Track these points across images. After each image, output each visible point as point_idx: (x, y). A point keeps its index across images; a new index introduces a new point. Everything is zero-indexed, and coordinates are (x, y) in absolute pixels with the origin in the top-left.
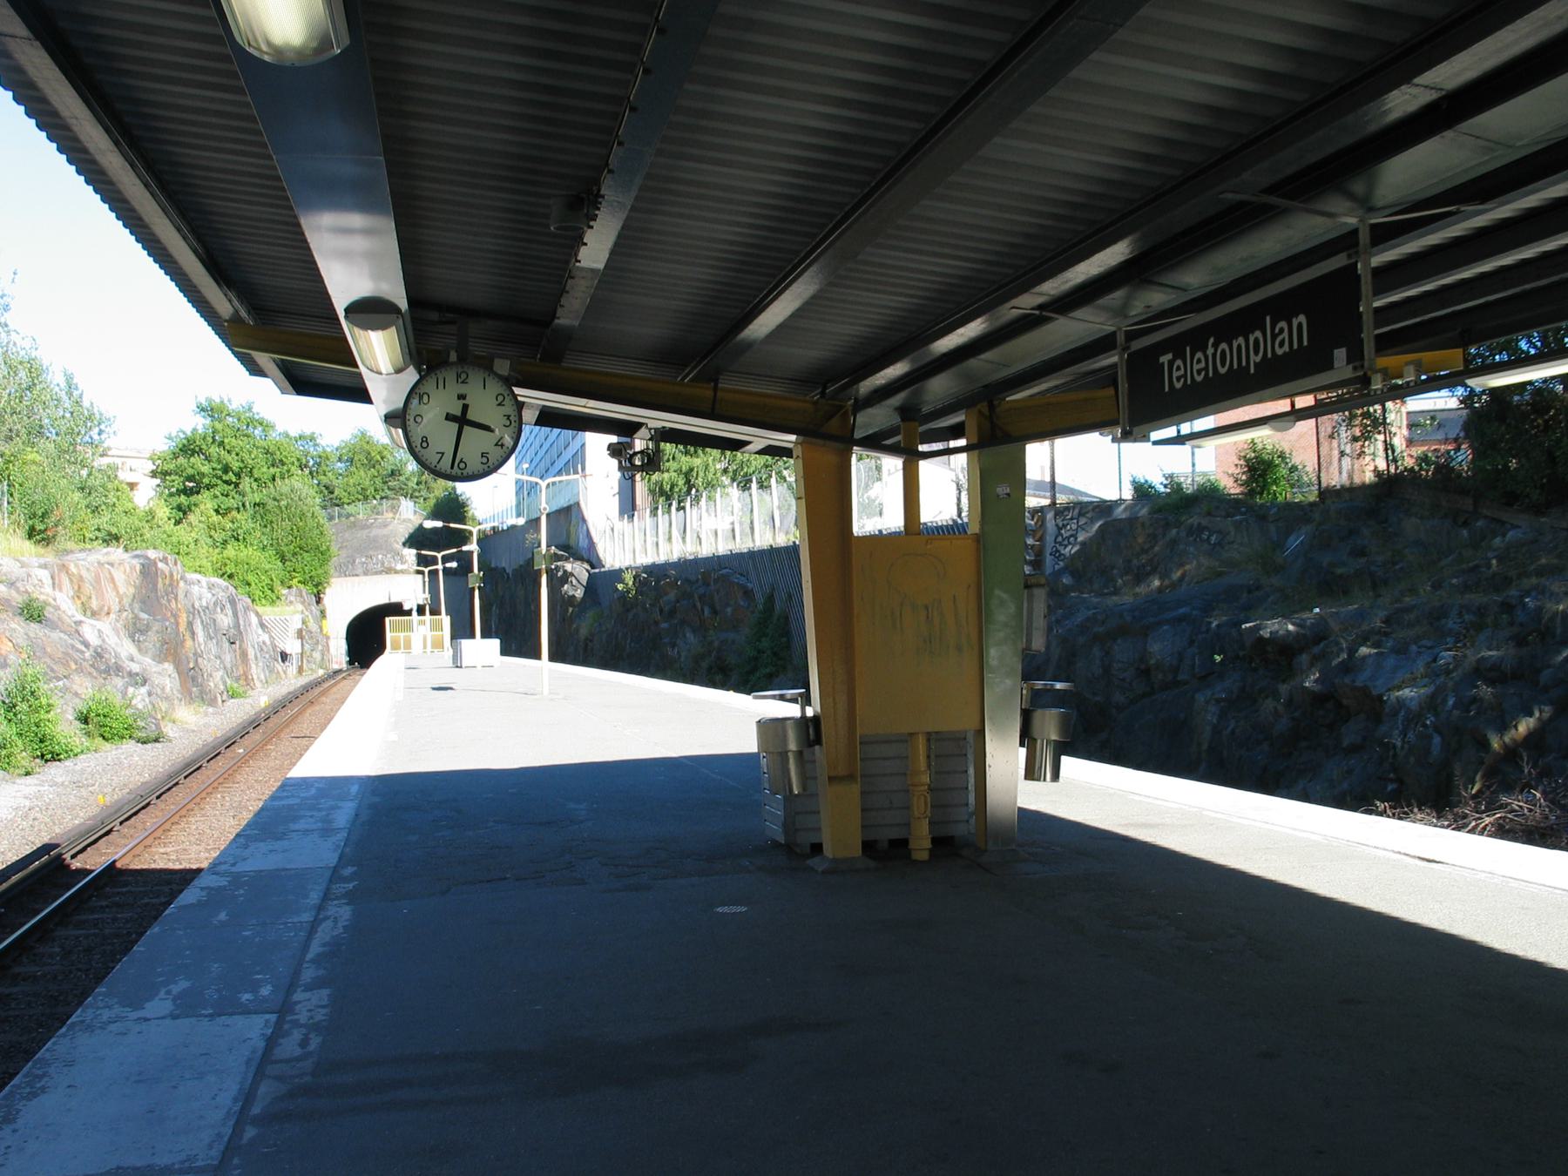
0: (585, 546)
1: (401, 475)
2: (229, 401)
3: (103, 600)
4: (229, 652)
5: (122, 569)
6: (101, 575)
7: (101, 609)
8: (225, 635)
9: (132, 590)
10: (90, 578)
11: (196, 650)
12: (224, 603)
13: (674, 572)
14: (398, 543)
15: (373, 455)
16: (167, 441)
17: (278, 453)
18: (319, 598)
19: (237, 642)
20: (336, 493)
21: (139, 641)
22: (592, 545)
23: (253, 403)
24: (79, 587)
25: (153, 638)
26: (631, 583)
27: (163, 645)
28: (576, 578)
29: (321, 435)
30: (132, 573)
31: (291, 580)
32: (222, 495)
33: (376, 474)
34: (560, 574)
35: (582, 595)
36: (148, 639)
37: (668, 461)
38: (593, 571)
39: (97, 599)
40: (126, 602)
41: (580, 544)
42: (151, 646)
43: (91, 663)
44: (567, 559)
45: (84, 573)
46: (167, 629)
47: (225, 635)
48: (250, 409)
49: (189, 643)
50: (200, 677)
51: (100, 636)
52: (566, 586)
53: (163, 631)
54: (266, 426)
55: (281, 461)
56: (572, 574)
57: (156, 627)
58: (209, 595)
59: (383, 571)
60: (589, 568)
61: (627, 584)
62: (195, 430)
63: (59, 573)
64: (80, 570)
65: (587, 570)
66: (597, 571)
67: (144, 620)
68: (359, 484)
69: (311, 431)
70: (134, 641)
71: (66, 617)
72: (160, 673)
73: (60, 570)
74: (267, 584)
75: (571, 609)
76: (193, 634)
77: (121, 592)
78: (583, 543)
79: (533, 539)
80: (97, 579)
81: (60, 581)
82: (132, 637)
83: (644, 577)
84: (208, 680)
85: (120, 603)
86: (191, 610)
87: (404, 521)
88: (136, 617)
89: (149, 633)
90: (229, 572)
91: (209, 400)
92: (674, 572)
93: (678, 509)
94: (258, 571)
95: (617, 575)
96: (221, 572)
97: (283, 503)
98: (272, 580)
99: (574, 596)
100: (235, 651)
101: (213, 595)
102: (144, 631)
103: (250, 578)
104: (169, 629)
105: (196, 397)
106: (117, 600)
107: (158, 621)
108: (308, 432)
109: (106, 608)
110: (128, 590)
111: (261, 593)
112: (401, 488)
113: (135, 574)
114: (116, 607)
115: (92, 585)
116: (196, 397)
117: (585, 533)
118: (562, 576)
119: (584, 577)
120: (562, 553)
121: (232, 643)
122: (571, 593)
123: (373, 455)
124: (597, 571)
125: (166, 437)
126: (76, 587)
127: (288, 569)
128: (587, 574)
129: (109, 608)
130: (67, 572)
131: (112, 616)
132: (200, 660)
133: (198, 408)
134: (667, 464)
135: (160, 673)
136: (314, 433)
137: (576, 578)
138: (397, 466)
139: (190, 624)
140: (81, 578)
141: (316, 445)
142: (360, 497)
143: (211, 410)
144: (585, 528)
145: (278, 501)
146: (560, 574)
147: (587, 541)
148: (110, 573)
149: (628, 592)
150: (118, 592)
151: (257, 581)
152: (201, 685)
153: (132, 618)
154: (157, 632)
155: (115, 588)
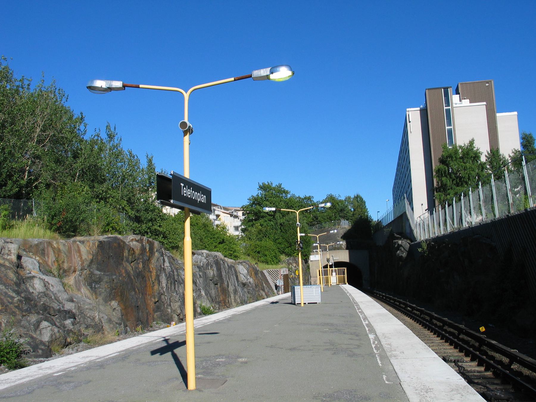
0: (409, 232)
1: (344, 211)
2: (271, 183)
3: (71, 263)
4: (214, 289)
5: (88, 244)
6: (72, 248)
7: (70, 268)
8: (211, 280)
9: (91, 257)
10: (64, 250)
11: (159, 291)
12: (212, 264)
13: (447, 240)
14: (339, 237)
15: (335, 204)
16: (249, 201)
17: (290, 203)
18: (307, 261)
19: (218, 284)
20: (319, 219)
21: (95, 288)
22: (411, 231)
23: (281, 184)
24: (58, 255)
25: (104, 287)
26: (426, 248)
27: (111, 290)
28: (403, 247)
29: (313, 197)
30: (93, 247)
31: (294, 254)
32: (269, 220)
33: (336, 211)
34: (396, 246)
35: (405, 256)
36: (101, 286)
37: (449, 189)
38: (411, 243)
39: (68, 262)
40: (86, 264)
41: (407, 231)
42: (103, 291)
43: (16, 305)
44: (400, 239)
45: (61, 247)
46: (113, 280)
47: (211, 280)
48: (280, 186)
49: (156, 287)
50: (163, 306)
51: (45, 286)
52: (398, 252)
53: (110, 282)
54: (286, 192)
55: (291, 206)
56: (401, 246)
57: (106, 279)
58: (205, 260)
59: (333, 249)
60: (410, 242)
61: (423, 249)
62: (258, 195)
63: (47, 247)
64: (59, 245)
65: (409, 243)
66: (413, 243)
67: (97, 275)
68: (328, 215)
69: (309, 195)
70: (91, 288)
71: (215, 272)
72: (90, 309)
73: (48, 246)
74: (274, 256)
75: (401, 263)
76: (159, 282)
77: (84, 258)
78: (408, 231)
79: (388, 231)
80: (70, 250)
81: (48, 252)
82: (90, 285)
83: (432, 244)
84: (167, 308)
85: (82, 264)
86: (159, 268)
87: (343, 228)
88: (92, 274)
89: (102, 283)
90: (258, 251)
91: (263, 184)
92: (447, 240)
93: (449, 206)
94: (270, 250)
95: (419, 245)
96: (254, 251)
97: (291, 222)
98: (276, 254)
99: (402, 256)
100: (217, 288)
101: (207, 260)
102: (99, 281)
103: (267, 253)
104: (115, 280)
105: (259, 183)
106: (80, 263)
107: (107, 275)
108: (308, 196)
109: (73, 268)
110: (88, 257)
111: (271, 259)
112: (344, 216)
113: (95, 247)
114: (79, 268)
115: (65, 254)
116: (259, 183)
117: (408, 226)
118: (397, 247)
119: (407, 246)
120: (398, 236)
121: (216, 284)
122: (400, 255)
123: (335, 204)
124: (413, 243)
125: (248, 200)
126: (57, 255)
127: (293, 249)
128: (409, 245)
129: (75, 268)
130: (52, 247)
131: (77, 273)
132: (163, 297)
133: (260, 187)
134: (448, 191)
135: (90, 309)
136: (310, 196)
137: (403, 247)
138: (342, 207)
139: (158, 277)
140: (59, 250)
141: (311, 201)
142: (328, 220)
143: (263, 187)
144: (408, 223)
145: (289, 222)
146: (396, 246)
147: (409, 229)
148: (78, 247)
149: (424, 253)
150: (81, 258)
151: (269, 254)
152: (163, 311)
153: (89, 274)
154: (107, 282)
155: (80, 256)
